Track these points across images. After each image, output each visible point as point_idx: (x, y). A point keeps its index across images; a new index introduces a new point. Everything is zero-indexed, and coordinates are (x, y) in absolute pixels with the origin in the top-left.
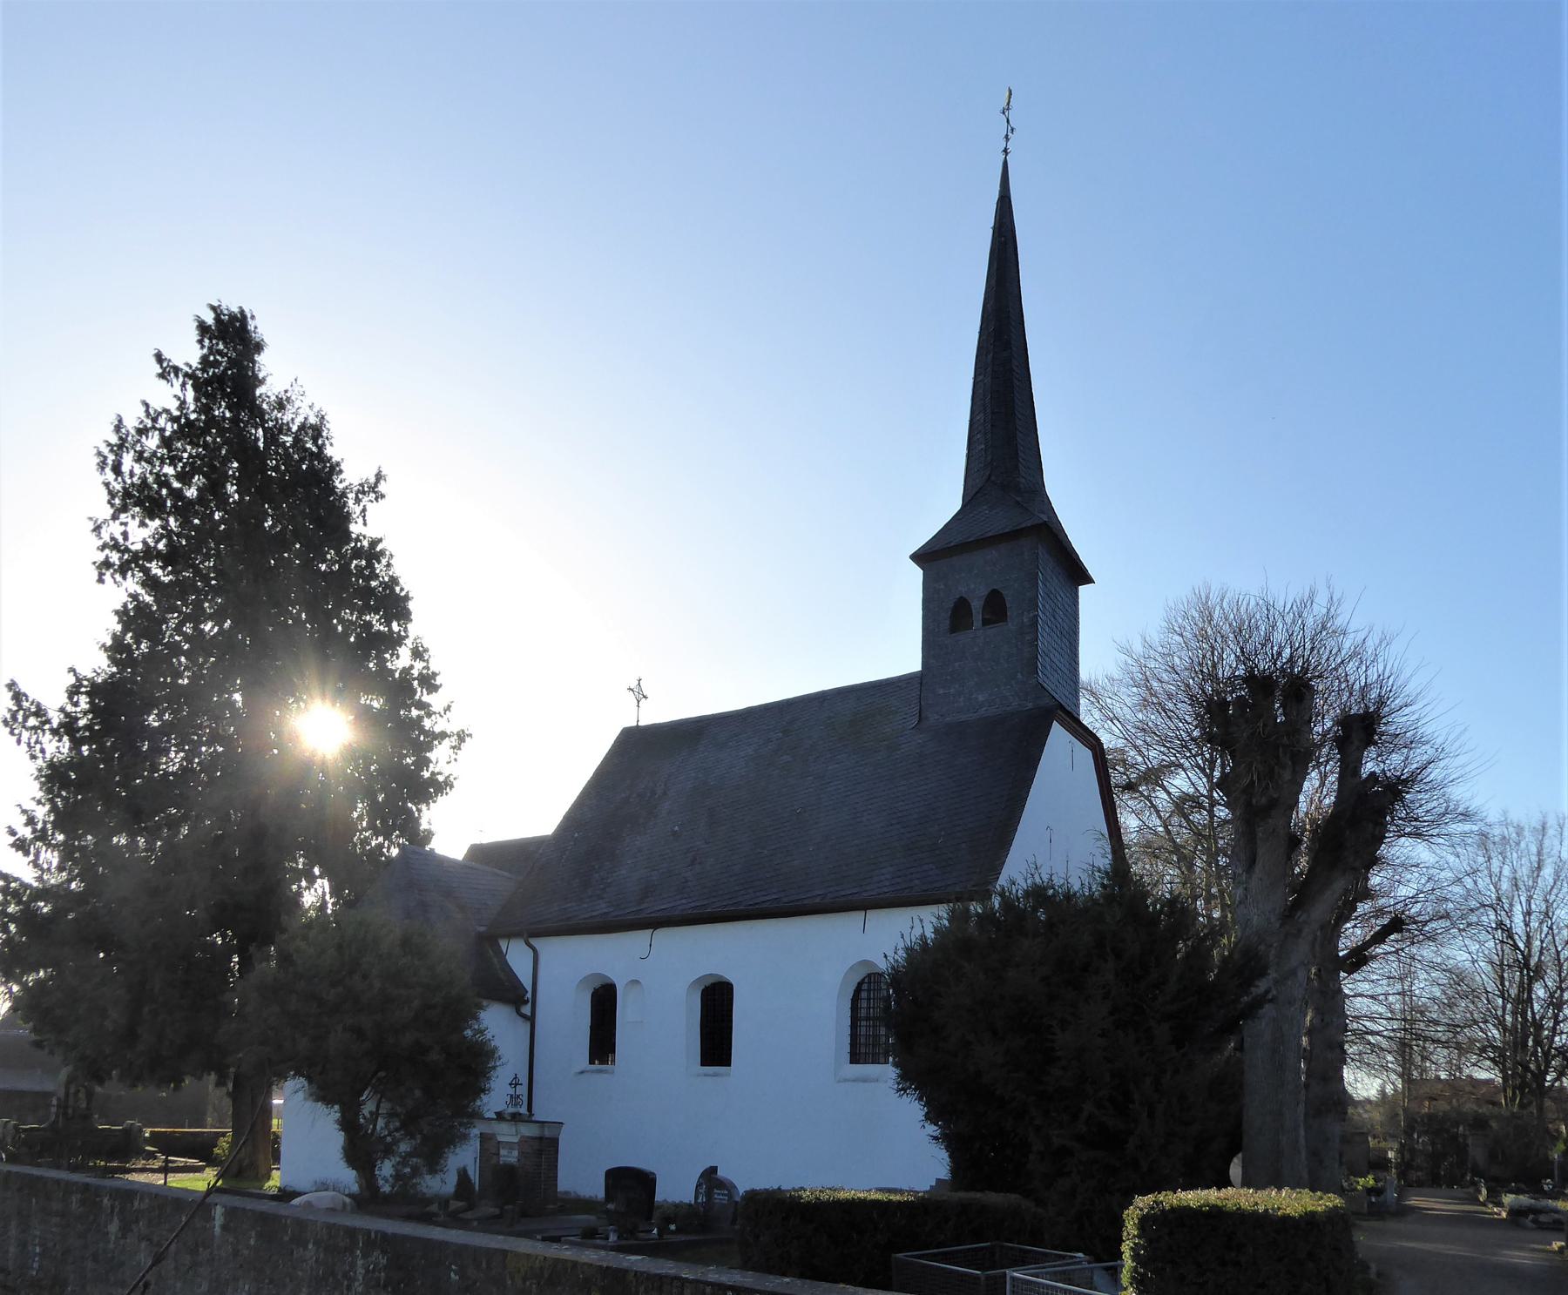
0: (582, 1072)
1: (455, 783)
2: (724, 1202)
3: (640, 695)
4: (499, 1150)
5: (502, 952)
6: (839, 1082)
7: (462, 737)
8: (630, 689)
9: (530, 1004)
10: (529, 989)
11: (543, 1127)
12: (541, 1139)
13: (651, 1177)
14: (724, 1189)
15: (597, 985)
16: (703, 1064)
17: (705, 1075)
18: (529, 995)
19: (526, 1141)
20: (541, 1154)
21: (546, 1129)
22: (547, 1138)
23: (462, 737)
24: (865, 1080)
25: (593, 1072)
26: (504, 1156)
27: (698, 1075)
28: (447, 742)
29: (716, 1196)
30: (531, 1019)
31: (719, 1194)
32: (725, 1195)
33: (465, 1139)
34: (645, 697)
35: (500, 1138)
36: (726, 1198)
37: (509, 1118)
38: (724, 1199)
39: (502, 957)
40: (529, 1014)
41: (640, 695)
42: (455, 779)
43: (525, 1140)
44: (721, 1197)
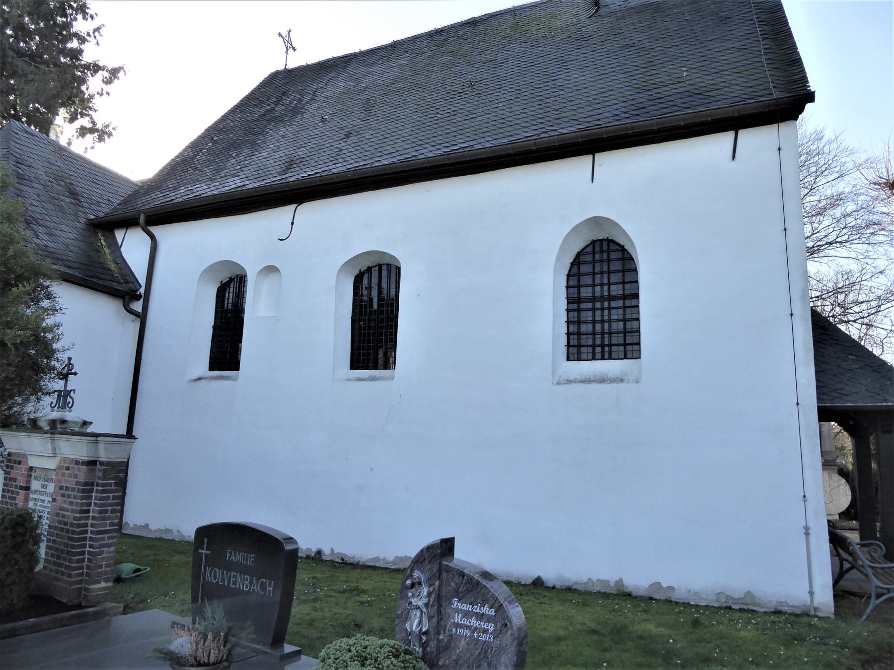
0: (200, 379)
1: (114, 133)
2: (483, 637)
3: (289, 46)
4: (29, 482)
5: (117, 242)
6: (558, 384)
7: (114, 73)
8: (280, 35)
9: (142, 300)
10: (142, 279)
11: (96, 442)
12: (92, 463)
13: (288, 547)
14: (484, 602)
15: (224, 277)
16: (352, 368)
17: (359, 379)
18: (142, 290)
19: (68, 468)
20: (91, 491)
21: (101, 446)
22: (102, 463)
23: (114, 73)
24: (602, 380)
25: (212, 378)
26: (36, 491)
27: (348, 380)
28: (100, 75)
29: (458, 618)
30: (142, 317)
31: (467, 614)
32: (489, 619)
33: (842, 469)
34: (294, 49)
35: (33, 462)
36: (491, 627)
37: (47, 428)
38: (485, 631)
39: (116, 248)
40: (140, 311)
41: (289, 46)
42: (114, 129)
43: (67, 466)
44: (474, 622)
